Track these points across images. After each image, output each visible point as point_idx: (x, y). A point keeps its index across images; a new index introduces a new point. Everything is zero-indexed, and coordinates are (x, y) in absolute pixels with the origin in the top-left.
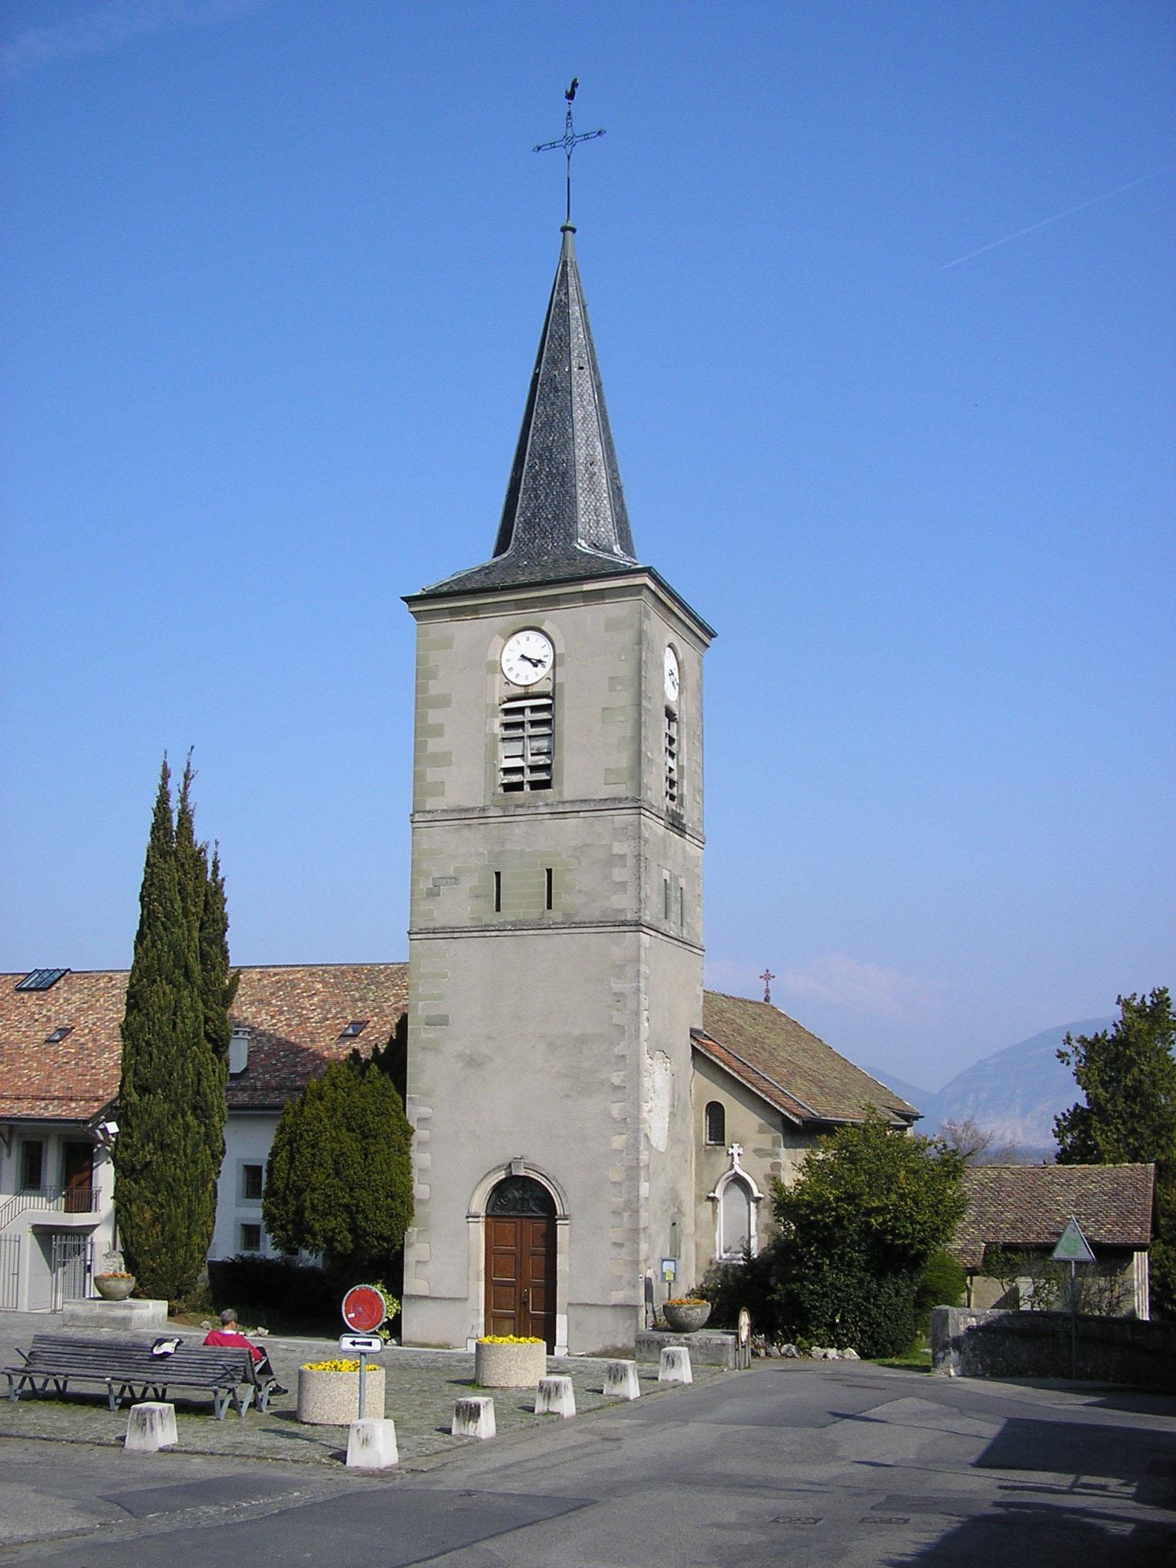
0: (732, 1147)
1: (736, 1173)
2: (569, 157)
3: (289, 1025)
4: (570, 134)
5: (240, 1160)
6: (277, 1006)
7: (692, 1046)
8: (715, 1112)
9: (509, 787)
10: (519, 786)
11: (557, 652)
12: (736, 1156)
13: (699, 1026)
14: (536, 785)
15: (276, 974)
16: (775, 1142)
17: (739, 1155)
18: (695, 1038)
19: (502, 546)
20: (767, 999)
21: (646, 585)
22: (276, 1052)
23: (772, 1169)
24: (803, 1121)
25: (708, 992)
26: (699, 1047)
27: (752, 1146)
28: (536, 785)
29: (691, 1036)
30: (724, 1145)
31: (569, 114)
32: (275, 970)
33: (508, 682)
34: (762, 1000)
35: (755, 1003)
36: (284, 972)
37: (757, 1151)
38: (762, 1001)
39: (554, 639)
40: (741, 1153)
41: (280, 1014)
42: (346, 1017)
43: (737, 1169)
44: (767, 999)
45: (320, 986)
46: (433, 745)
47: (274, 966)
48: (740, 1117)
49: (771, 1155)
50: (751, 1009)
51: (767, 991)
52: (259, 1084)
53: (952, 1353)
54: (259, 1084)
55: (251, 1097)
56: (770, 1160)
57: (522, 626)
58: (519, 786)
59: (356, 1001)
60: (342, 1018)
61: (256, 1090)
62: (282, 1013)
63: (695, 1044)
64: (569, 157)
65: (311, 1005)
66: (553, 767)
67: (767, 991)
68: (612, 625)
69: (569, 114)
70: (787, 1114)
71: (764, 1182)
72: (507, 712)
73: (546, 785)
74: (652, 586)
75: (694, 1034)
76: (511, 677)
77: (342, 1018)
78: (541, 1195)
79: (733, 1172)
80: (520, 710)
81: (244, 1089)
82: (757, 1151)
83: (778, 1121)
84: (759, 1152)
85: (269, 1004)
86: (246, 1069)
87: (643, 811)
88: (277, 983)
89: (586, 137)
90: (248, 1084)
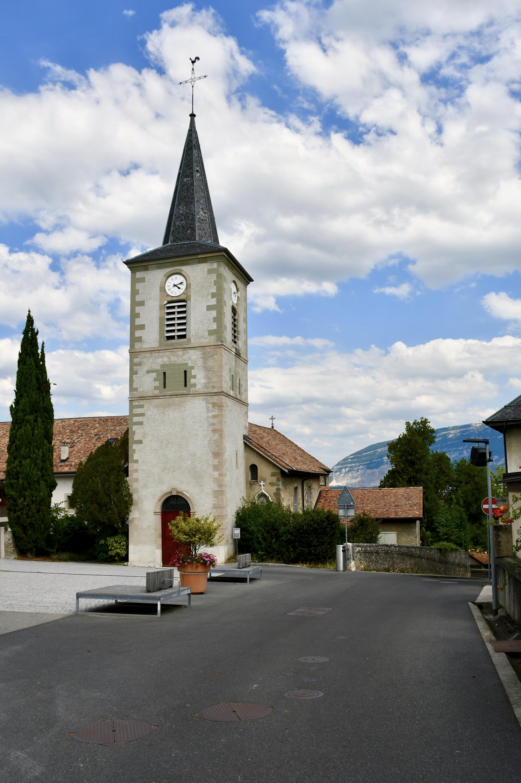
0: (261, 482)
1: (262, 492)
2: (193, 86)
3: (85, 441)
4: (193, 77)
5: (66, 494)
6: (81, 433)
7: (244, 442)
8: (253, 469)
9: (169, 338)
10: (173, 337)
11: (188, 283)
12: (262, 486)
13: (247, 434)
14: (180, 337)
15: (81, 421)
16: (278, 480)
17: (263, 485)
18: (245, 439)
19: (166, 241)
20: (273, 427)
21: (223, 255)
22: (80, 451)
23: (277, 491)
24: (288, 471)
25: (250, 423)
26: (247, 443)
27: (268, 481)
28: (180, 337)
29: (244, 438)
30: (257, 481)
31: (193, 69)
32: (80, 420)
33: (168, 295)
34: (271, 428)
35: (268, 428)
36: (84, 420)
37: (270, 483)
38: (271, 428)
39: (185, 275)
40: (264, 484)
41: (82, 437)
42: (108, 437)
43: (263, 490)
44: (273, 427)
45: (97, 425)
46: (138, 322)
47: (80, 418)
48: (264, 470)
49: (276, 485)
50: (267, 431)
51: (272, 424)
52: (73, 464)
53: (352, 562)
54: (73, 464)
55: (70, 469)
56: (275, 487)
57: (173, 272)
58: (173, 337)
59: (112, 430)
60: (106, 437)
61: (72, 466)
62: (82, 436)
63: (245, 441)
64: (193, 86)
65: (94, 433)
66: (187, 330)
67: (272, 424)
68: (210, 271)
69: (193, 69)
70: (283, 468)
71: (273, 496)
72: (168, 308)
73: (184, 336)
74: (226, 256)
75: (245, 437)
76: (169, 293)
77: (106, 437)
78: (184, 503)
79: (261, 492)
80: (173, 307)
81: (67, 466)
82: (270, 483)
83: (278, 471)
84: (271, 484)
85: (78, 433)
86: (68, 458)
87: (223, 346)
88: (81, 424)
89: (200, 78)
90: (69, 464)
